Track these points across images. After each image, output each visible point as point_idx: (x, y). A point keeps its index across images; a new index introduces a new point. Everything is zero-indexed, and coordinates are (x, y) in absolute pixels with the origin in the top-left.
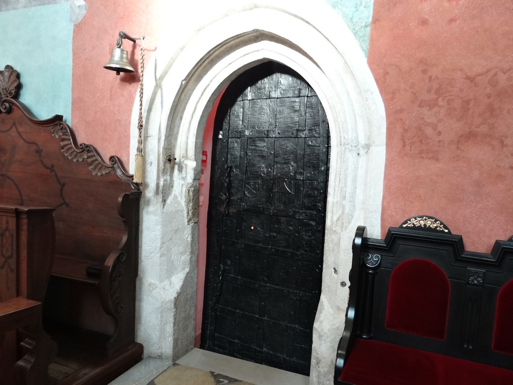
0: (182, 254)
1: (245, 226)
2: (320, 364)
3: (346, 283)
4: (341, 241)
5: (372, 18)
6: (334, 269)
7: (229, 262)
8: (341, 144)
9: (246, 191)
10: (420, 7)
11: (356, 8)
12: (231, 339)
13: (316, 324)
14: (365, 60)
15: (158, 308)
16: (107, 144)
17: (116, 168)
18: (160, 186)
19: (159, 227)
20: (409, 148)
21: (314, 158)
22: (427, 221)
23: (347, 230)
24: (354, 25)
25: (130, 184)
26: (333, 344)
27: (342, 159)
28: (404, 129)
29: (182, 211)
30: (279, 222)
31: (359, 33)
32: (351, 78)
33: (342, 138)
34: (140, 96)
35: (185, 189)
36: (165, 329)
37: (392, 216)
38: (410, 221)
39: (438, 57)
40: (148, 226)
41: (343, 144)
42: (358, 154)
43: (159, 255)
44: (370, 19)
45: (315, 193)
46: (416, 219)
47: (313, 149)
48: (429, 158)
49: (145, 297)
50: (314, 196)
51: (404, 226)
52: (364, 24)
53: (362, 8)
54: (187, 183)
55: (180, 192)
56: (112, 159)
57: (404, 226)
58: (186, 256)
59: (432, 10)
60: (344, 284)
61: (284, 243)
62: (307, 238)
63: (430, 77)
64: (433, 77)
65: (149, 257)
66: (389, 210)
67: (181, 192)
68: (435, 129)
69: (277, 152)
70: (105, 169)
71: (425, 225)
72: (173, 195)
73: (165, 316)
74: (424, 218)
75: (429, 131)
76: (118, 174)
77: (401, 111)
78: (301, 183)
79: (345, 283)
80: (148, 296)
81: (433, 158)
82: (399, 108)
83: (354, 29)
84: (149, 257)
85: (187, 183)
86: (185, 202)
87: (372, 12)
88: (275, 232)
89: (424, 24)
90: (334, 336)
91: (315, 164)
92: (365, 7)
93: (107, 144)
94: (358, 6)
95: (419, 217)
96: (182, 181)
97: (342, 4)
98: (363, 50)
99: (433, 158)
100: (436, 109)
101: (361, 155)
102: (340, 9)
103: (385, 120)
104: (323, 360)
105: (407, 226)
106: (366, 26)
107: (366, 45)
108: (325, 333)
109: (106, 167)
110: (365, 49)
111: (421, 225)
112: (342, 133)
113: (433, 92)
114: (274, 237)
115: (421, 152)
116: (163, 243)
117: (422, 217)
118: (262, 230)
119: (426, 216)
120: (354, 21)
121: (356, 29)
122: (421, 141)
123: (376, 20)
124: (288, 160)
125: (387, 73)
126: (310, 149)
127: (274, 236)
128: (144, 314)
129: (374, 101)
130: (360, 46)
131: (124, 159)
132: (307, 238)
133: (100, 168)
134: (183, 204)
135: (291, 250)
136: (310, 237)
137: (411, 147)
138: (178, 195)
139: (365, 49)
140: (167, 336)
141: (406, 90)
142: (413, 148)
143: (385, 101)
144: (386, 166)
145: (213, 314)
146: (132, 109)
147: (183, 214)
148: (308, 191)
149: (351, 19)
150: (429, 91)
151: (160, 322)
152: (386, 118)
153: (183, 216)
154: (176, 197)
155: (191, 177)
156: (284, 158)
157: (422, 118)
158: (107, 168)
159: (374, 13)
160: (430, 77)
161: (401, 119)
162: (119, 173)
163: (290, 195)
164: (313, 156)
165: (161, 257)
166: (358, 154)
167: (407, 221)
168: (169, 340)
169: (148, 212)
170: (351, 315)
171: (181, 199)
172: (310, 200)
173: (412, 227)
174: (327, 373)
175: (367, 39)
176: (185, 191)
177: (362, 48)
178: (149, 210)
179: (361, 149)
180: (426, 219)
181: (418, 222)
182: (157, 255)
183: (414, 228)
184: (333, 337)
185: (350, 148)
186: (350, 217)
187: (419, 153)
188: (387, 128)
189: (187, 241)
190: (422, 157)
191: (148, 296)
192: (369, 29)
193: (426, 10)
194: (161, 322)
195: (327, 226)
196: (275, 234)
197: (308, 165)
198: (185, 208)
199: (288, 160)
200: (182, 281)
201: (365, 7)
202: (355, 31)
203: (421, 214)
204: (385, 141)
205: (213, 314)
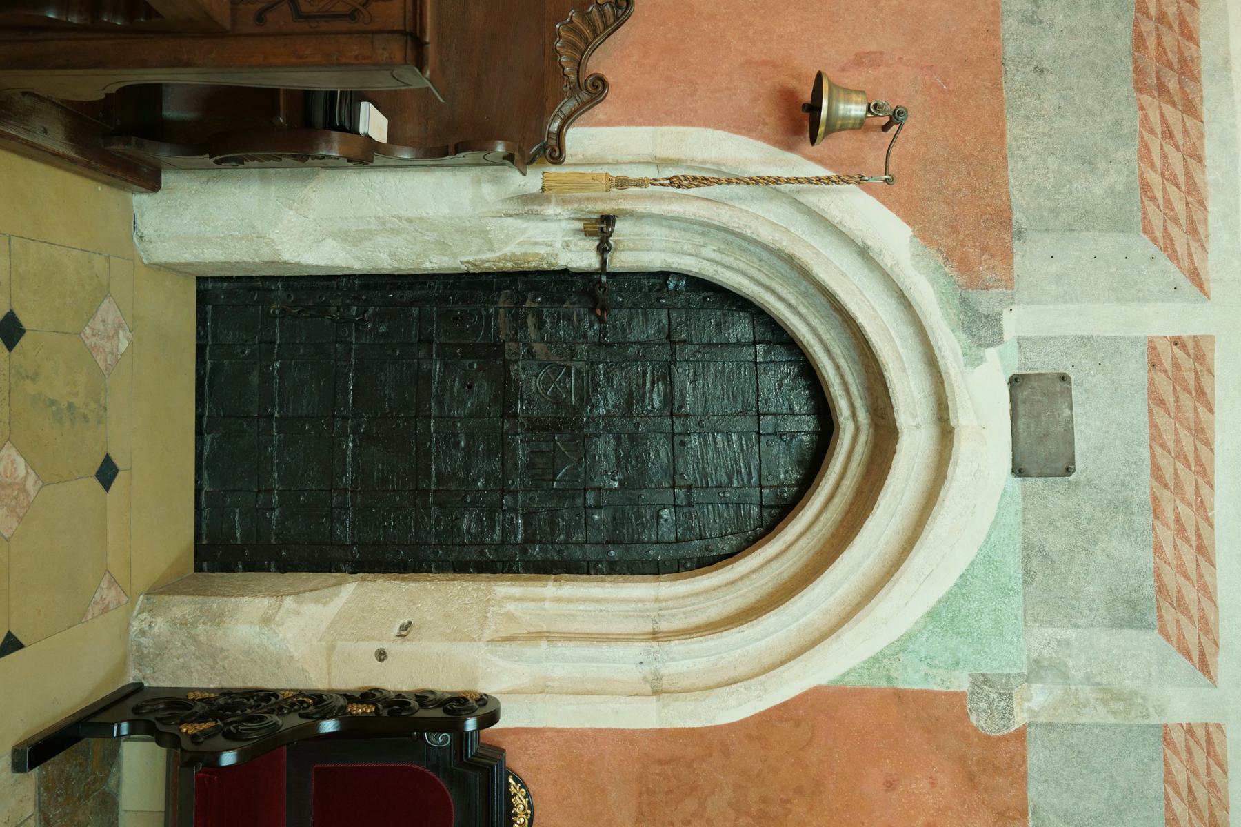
0: (393, 255)
1: (471, 365)
2: (211, 626)
3: (385, 662)
4: (468, 643)
5: (905, 690)
6: (410, 623)
7: (382, 329)
8: (661, 610)
9: (551, 367)
10: (918, 776)
11: (926, 658)
12: (208, 349)
13: (291, 602)
14: (823, 681)
15: (254, 227)
16: (635, 58)
17: (579, 100)
18: (542, 207)
19: (445, 210)
20: (657, 771)
21: (633, 529)
22: (524, 816)
23: (489, 656)
24: (893, 655)
25: (541, 141)
26: (257, 649)
27: (631, 613)
28: (693, 760)
29: (491, 250)
30: (489, 453)
31: (877, 665)
32: (790, 643)
33: (673, 611)
34: (751, 179)
35: (542, 252)
36: (208, 246)
37: (527, 749)
38: (520, 788)
39: (826, 813)
40: (445, 185)
41: (661, 612)
42: (641, 663)
43: (380, 214)
44: (901, 686)
45: (560, 534)
46: (525, 798)
47: (652, 526)
48: (639, 807)
49: (273, 188)
50: (554, 532)
51: (511, 780)
52: (893, 673)
53: (924, 668)
54: (557, 255)
55: (533, 239)
56: (600, 83)
57: (511, 780)
58: (390, 261)
59: (913, 797)
60: (382, 657)
61: (446, 468)
62: (465, 527)
63: (788, 801)
64: (789, 806)
65: (371, 191)
66: (537, 742)
67: (536, 243)
68: (693, 815)
69: (642, 439)
70: (572, 59)
71: (516, 814)
72: (524, 225)
73: (238, 246)
74: (529, 812)
75: (690, 805)
76: (562, 103)
77: (726, 753)
78: (579, 501)
79: (383, 660)
80: (278, 197)
81: (642, 813)
82: (732, 749)
83: (884, 657)
84: (371, 191)
85: (557, 255)
86: (513, 254)
87: (916, 688)
88: (467, 445)
89: (888, 785)
90: (275, 653)
91: (620, 532)
92: (926, 674)
93: (635, 58)
94: (929, 661)
95: (529, 802)
96: (561, 243)
97: (936, 629)
98: (843, 676)
99: (642, 813)
100: (732, 815)
101: (641, 668)
102: (925, 627)
103: (709, 725)
104: (220, 632)
105: (510, 783)
106: (889, 678)
107: (853, 682)
108: (276, 633)
109: (580, 63)
110: (846, 679)
111: (516, 807)
112: (684, 609)
113: (762, 806)
114: (457, 444)
115: (650, 792)
116: (409, 220)
117: (530, 808)
118: (466, 412)
119: (532, 815)
120: (901, 656)
121: (885, 661)
122: (671, 791)
123: (900, 696)
124: (626, 465)
125: (798, 723)
126: (652, 517)
127: (459, 443)
128: (233, 189)
129: (745, 703)
130: (851, 669)
131: (600, 110)
132: (465, 527)
133: (574, 46)
134: (508, 250)
135: (434, 488)
136: (468, 531)
137: (657, 774)
138: (526, 235)
139: (846, 679)
140: (195, 251)
141: (765, 760)
142: (658, 777)
143: (746, 722)
144: (622, 731)
145: (255, 299)
146: (723, 129)
147: (484, 252)
148: (563, 519)
149: (905, 650)
150: (764, 800)
151: (222, 235)
152: (711, 727)
153: (479, 252)
154: (524, 231)
155: (572, 260)
156: (630, 457)
157: (713, 793)
158: (576, 67)
159: (913, 692)
160: (788, 801)
161: (711, 755)
162: (568, 106)
163: (551, 477)
164: (637, 525)
165: (375, 217)
166: (641, 663)
167: (521, 783)
168: (186, 255)
169: (477, 182)
170: (325, 726)
171: (518, 244)
172: (544, 523)
173: (510, 792)
174: (196, 641)
175: (866, 682)
176: (539, 254)
177: (848, 673)
178: (482, 185)
179: (652, 667)
180: (526, 814)
181: (520, 802)
182: (379, 209)
183: (509, 796)
184: (272, 648)
185: (652, 650)
186: (517, 658)
187: (648, 789)
188: (693, 729)
189: (424, 262)
190: (641, 794)
191: (278, 197)
192: (884, 684)
193: (913, 786)
194: (222, 238)
195: (495, 588)
196: (462, 444)
197: (618, 515)
198: (498, 254)
199: (626, 465)
200: (329, 263)
201: (926, 674)
202: (880, 657)
203: (535, 803)
204: (668, 727)
205: (255, 299)
